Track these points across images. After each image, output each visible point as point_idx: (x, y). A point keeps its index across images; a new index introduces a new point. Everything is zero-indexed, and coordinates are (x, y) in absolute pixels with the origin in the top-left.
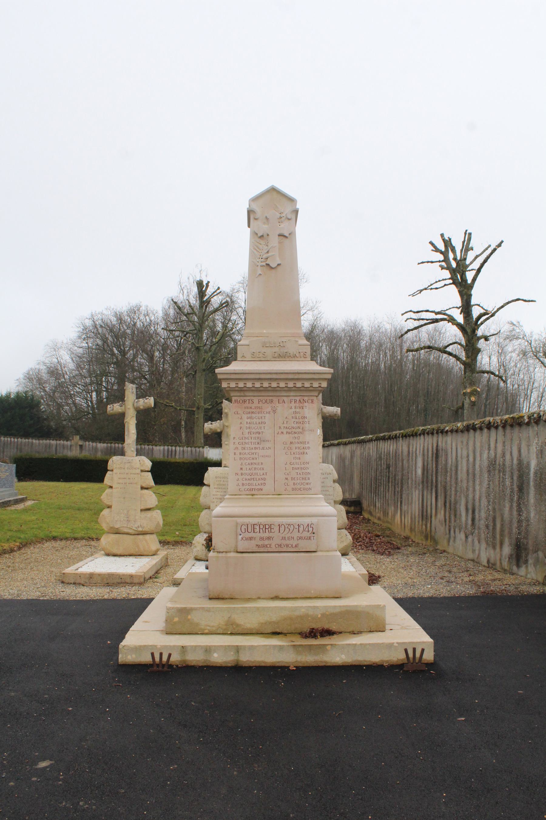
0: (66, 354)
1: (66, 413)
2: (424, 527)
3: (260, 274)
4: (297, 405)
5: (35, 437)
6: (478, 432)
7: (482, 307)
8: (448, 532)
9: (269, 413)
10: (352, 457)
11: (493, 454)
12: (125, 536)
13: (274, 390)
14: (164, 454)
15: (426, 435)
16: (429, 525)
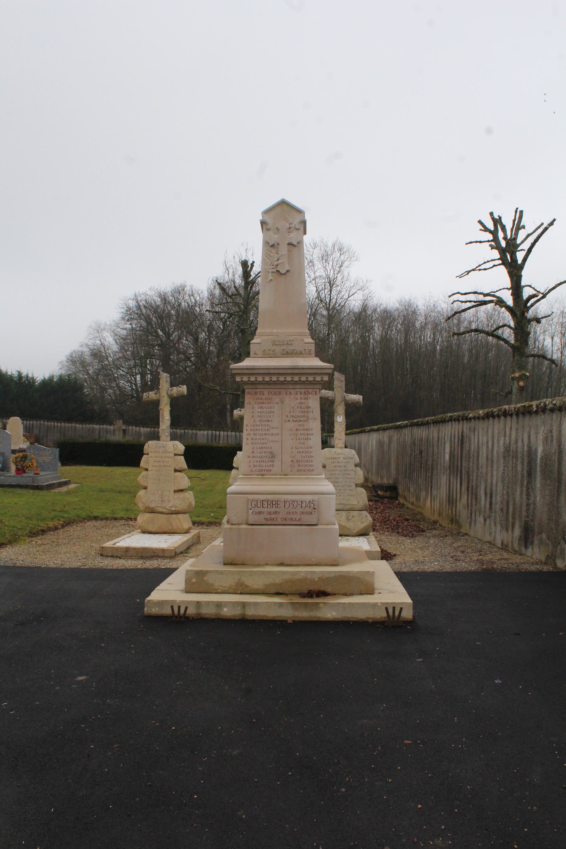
0: (109, 335)
1: (110, 396)
2: (450, 511)
3: (271, 280)
4: (303, 396)
5: (77, 420)
6: (496, 419)
7: (534, 288)
8: (470, 515)
9: (277, 403)
10: (390, 442)
11: (508, 441)
12: (159, 515)
13: (282, 383)
14: (208, 438)
15: (453, 422)
16: (454, 509)
